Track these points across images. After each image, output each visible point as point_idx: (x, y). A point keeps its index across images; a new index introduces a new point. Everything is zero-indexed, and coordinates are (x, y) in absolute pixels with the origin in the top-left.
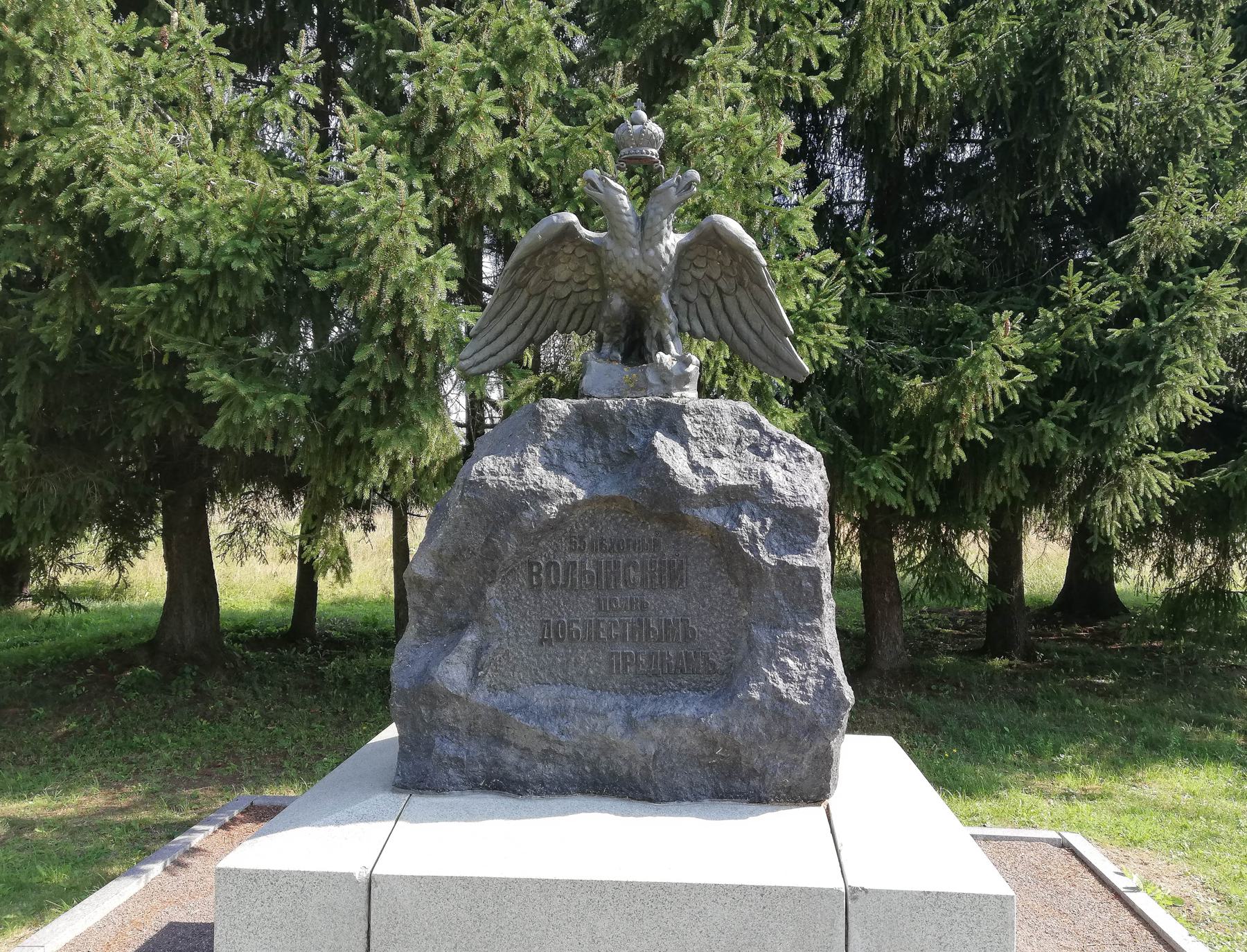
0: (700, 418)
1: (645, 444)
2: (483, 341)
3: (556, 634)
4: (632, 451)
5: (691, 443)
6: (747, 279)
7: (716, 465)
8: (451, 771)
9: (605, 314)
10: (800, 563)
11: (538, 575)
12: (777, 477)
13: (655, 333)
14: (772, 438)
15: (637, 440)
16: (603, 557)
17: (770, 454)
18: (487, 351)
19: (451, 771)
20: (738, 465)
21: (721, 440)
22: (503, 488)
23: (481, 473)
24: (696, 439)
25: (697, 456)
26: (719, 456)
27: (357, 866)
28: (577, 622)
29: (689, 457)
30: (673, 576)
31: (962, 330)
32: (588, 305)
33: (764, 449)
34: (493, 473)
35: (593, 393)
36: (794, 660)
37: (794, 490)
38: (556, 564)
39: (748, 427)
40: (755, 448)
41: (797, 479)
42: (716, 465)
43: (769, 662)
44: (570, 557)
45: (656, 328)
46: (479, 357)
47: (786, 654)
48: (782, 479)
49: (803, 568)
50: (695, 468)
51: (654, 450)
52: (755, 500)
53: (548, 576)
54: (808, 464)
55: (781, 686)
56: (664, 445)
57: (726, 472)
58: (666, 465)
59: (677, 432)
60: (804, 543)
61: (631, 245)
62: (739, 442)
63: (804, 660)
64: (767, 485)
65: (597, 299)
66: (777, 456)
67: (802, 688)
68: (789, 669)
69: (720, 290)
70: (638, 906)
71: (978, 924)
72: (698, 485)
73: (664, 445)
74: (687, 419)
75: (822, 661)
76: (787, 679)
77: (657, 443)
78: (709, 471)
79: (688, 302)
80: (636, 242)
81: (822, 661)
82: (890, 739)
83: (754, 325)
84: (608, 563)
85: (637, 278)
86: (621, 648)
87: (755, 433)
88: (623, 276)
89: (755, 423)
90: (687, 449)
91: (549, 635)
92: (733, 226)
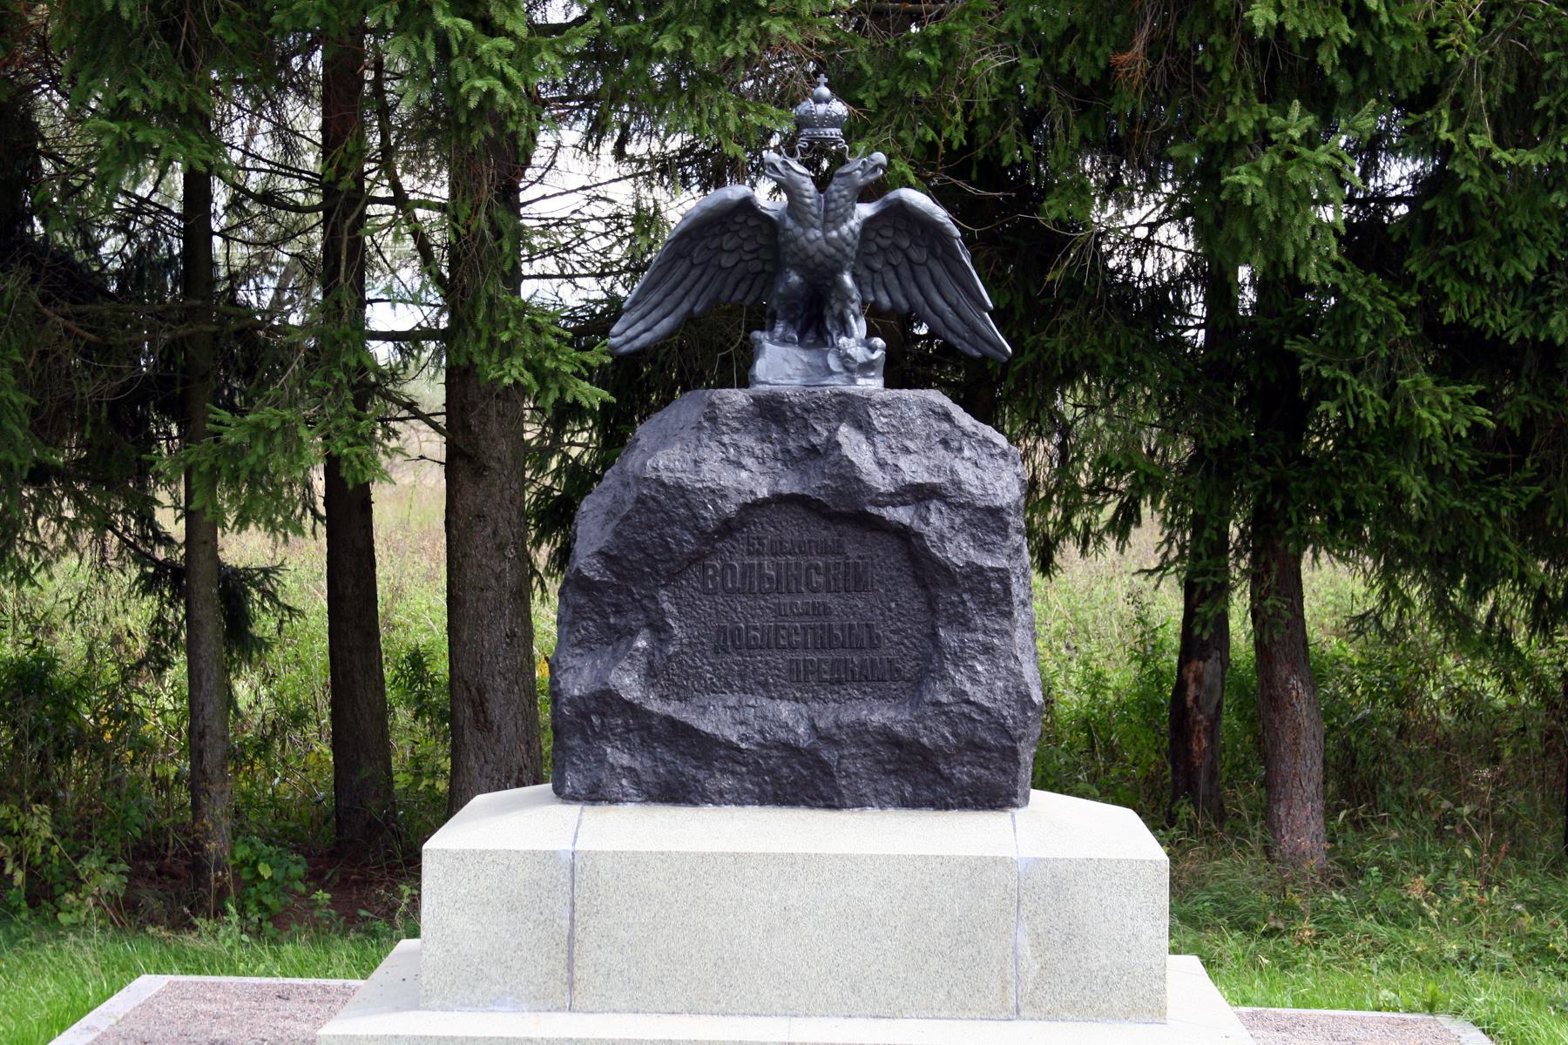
0: (886, 411)
1: (828, 440)
2: (636, 315)
3: (733, 642)
4: (814, 446)
5: (878, 439)
6: (939, 251)
7: (904, 462)
8: (624, 782)
9: (781, 290)
10: (989, 564)
11: (713, 578)
12: (966, 473)
13: (836, 312)
14: (964, 434)
15: (819, 435)
16: (782, 560)
17: (960, 450)
18: (640, 326)
19: (624, 782)
20: (925, 461)
21: (912, 436)
22: (56, 446)
23: (656, 469)
24: (883, 434)
25: (883, 452)
26: (907, 451)
27: (563, 845)
28: (756, 629)
29: (875, 453)
30: (855, 581)
31: (596, 699)
32: (758, 274)
33: (955, 444)
34: (667, 469)
35: (770, 379)
36: (982, 663)
37: (985, 489)
38: (732, 567)
39: (940, 420)
40: (945, 443)
41: (988, 476)
42: (904, 462)
43: (956, 665)
44: (747, 561)
45: (837, 307)
46: (630, 333)
47: (974, 658)
48: (972, 477)
49: (993, 569)
50: (882, 465)
51: (838, 445)
52: (943, 498)
53: (724, 579)
54: (1001, 462)
55: (968, 687)
56: (847, 436)
57: (914, 470)
58: (851, 462)
59: (865, 427)
60: (994, 543)
61: (813, 226)
62: (928, 436)
63: (993, 663)
64: (958, 484)
65: (768, 268)
66: (967, 453)
67: (990, 691)
68: (977, 672)
69: (909, 260)
70: (827, 875)
71: (1135, 886)
72: (880, 481)
73: (847, 436)
74: (872, 412)
75: (1012, 664)
76: (974, 681)
77: (841, 439)
78: (897, 468)
79: (872, 271)
80: (818, 223)
81: (1012, 664)
82: (1130, 811)
83: (949, 297)
84: (788, 565)
85: (819, 258)
86: (799, 656)
87: (946, 426)
88: (802, 255)
89: (947, 417)
90: (874, 445)
91: (725, 641)
92: (918, 199)
